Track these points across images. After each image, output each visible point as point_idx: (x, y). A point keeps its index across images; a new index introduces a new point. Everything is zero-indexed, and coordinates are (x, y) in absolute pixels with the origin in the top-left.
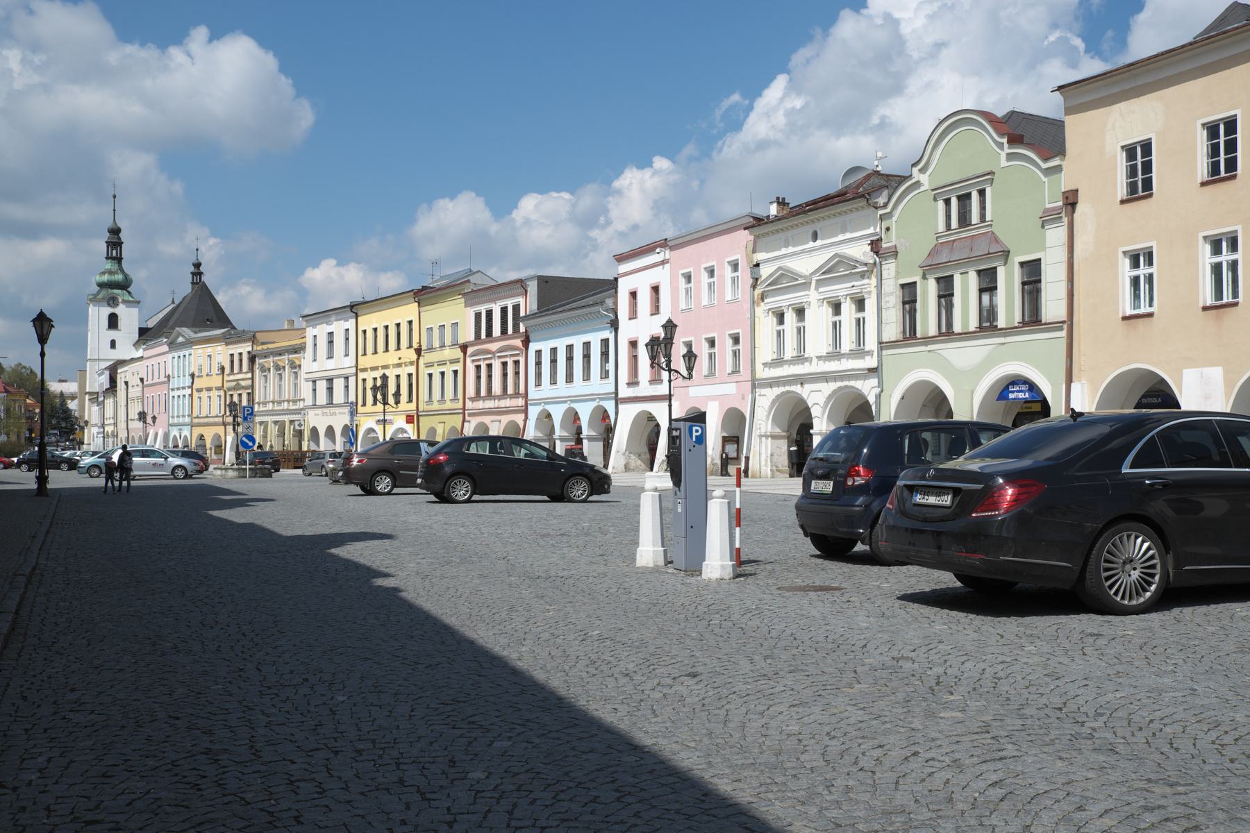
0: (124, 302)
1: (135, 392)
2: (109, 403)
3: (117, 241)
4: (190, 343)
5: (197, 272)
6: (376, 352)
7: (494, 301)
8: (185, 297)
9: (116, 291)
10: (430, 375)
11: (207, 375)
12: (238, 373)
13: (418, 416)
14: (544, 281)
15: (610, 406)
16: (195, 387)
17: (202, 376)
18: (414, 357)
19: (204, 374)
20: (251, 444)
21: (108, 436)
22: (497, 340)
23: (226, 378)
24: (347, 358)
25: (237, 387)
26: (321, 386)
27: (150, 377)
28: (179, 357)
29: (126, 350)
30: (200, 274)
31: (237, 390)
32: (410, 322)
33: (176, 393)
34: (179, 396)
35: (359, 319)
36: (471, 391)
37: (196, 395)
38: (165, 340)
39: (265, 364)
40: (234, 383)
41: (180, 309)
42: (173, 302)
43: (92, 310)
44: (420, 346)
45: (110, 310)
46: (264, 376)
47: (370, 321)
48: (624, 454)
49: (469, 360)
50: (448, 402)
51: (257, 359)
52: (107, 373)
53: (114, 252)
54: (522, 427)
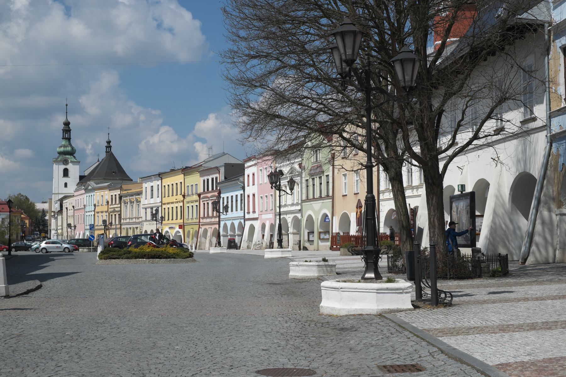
0: (71, 162)
1: (71, 213)
2: (59, 218)
3: (67, 129)
4: (94, 189)
5: (109, 146)
6: (169, 196)
7: (209, 175)
8: (103, 159)
9: (67, 156)
10: (188, 207)
11: (101, 205)
12: (114, 204)
13: (184, 225)
14: (227, 166)
16: (96, 211)
17: (99, 206)
18: (182, 199)
19: (100, 204)
20: (93, 239)
21: (59, 235)
22: (211, 192)
24: (158, 198)
28: (89, 196)
29: (71, 189)
30: (110, 147)
31: (114, 212)
32: (181, 183)
33: (88, 214)
34: (89, 215)
35: (163, 180)
36: (202, 215)
37: (96, 215)
38: (83, 188)
39: (126, 200)
40: (113, 209)
41: (101, 164)
43: (55, 167)
44: (185, 194)
45: (64, 167)
46: (126, 206)
47: (168, 181)
48: (247, 242)
49: (201, 200)
50: (190, 220)
51: (122, 198)
52: (59, 202)
53: (67, 135)
54: (218, 229)
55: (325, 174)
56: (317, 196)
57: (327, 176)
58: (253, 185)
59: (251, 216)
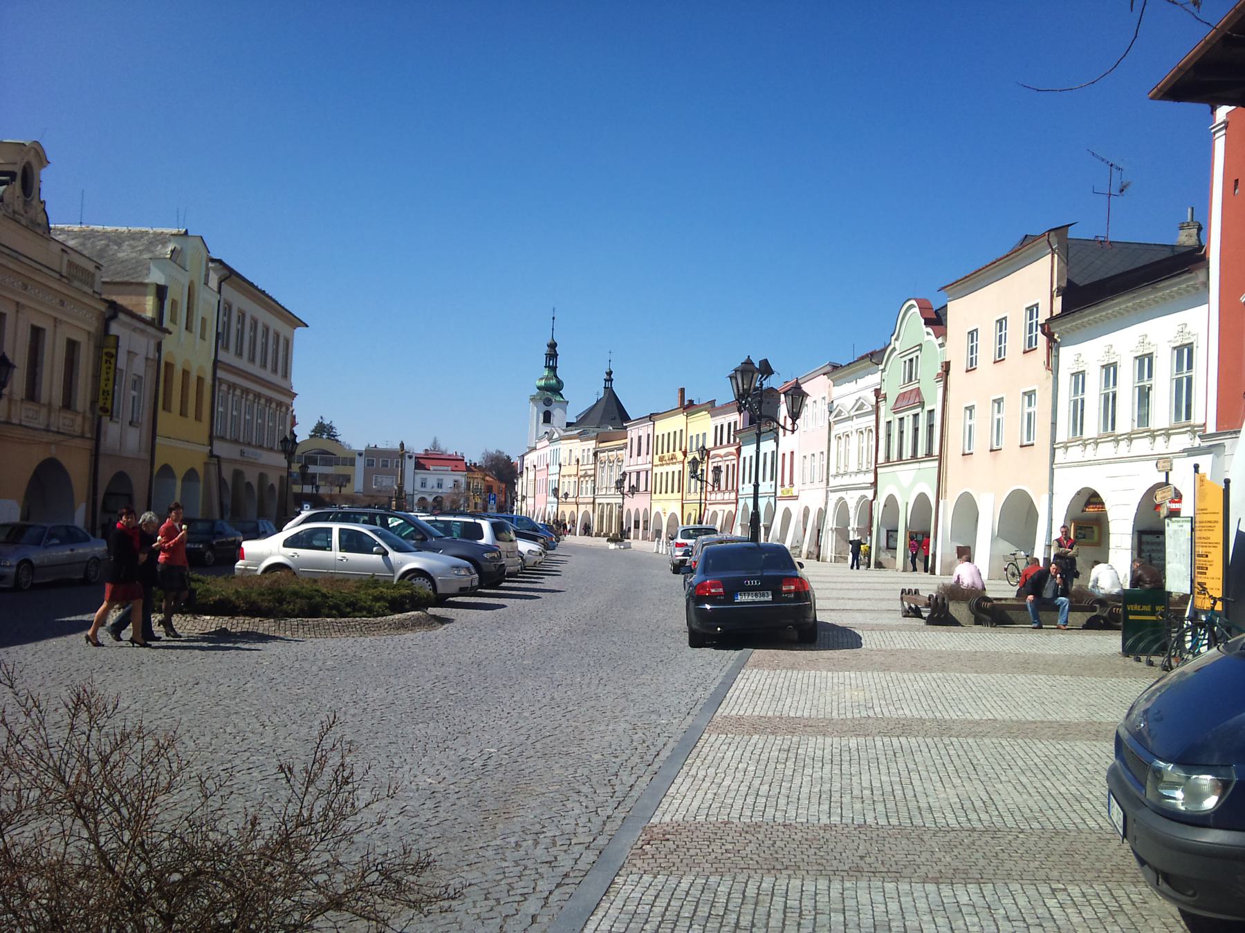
5: (609, 379)
23: (580, 468)
40: (584, 472)
45: (546, 408)
53: (551, 362)
55: (927, 408)
56: (907, 456)
57: (931, 412)
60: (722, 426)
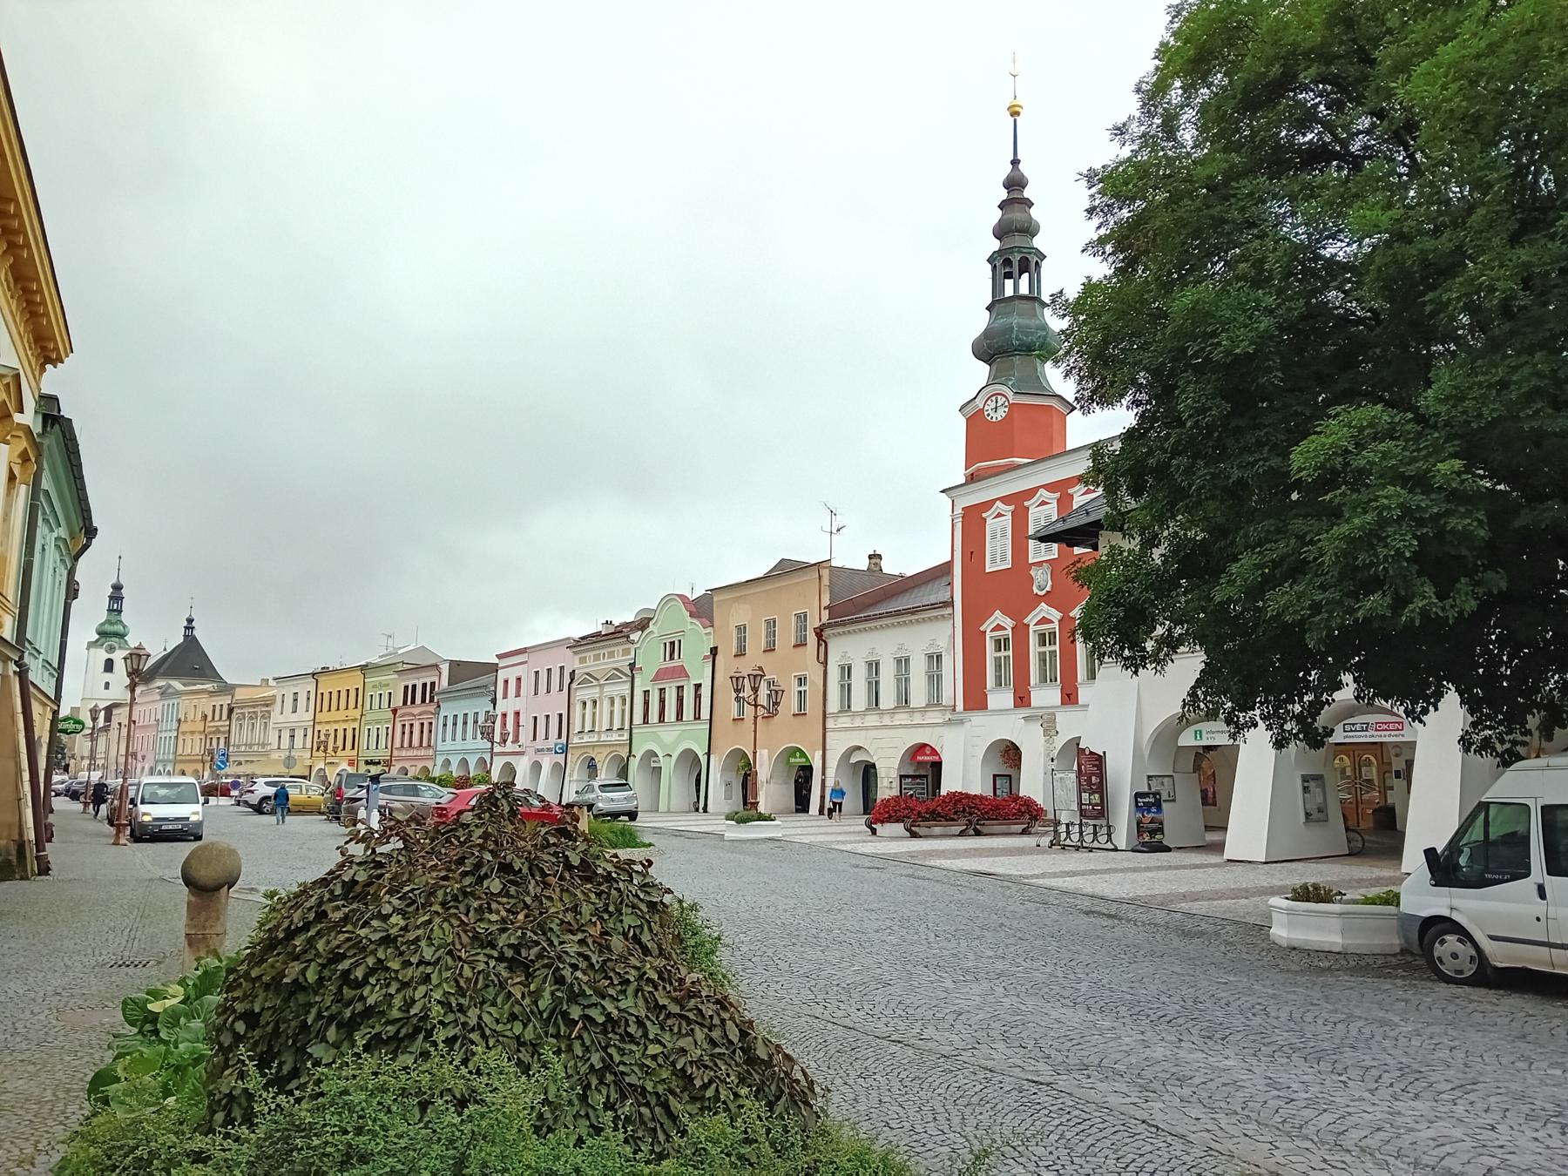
5: (189, 627)
15: (487, 757)
22: (419, 706)
25: (218, 731)
26: (286, 735)
27: (142, 720)
33: (163, 735)
36: (397, 744)
37: (181, 738)
42: (165, 650)
49: (397, 720)
57: (698, 686)
58: (518, 695)
59: (510, 747)
60: (414, 687)
